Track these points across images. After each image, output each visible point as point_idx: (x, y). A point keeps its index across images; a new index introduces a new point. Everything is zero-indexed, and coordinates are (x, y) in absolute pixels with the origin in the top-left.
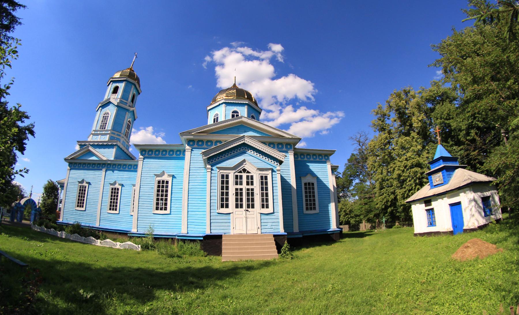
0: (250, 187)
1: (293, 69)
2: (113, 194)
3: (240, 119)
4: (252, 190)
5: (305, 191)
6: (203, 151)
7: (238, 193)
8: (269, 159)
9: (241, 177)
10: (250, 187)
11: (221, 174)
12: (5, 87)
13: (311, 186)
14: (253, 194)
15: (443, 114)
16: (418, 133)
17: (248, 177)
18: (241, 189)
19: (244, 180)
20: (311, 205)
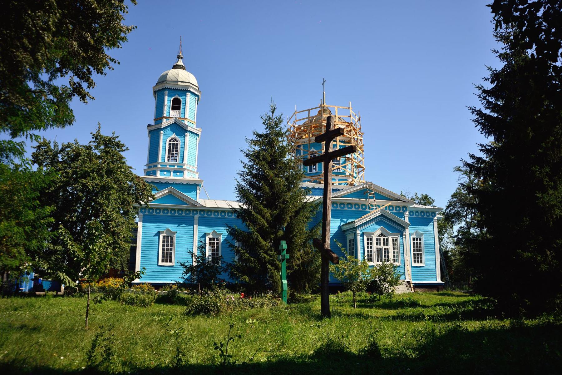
0: (386, 247)
1: (67, 187)
2: (416, 252)
3: (266, 255)
4: (388, 249)
5: (414, 250)
6: (535, 54)
7: (379, 251)
8: (493, 116)
9: (380, 239)
10: (386, 247)
11: (160, 263)
12: (315, 298)
13: (215, 253)
14: (388, 252)
15: (288, 261)
16: (69, 173)
17: (384, 239)
18: (381, 249)
19: (382, 242)
20: (418, 258)
